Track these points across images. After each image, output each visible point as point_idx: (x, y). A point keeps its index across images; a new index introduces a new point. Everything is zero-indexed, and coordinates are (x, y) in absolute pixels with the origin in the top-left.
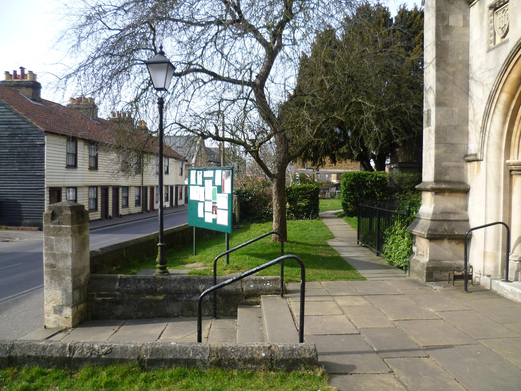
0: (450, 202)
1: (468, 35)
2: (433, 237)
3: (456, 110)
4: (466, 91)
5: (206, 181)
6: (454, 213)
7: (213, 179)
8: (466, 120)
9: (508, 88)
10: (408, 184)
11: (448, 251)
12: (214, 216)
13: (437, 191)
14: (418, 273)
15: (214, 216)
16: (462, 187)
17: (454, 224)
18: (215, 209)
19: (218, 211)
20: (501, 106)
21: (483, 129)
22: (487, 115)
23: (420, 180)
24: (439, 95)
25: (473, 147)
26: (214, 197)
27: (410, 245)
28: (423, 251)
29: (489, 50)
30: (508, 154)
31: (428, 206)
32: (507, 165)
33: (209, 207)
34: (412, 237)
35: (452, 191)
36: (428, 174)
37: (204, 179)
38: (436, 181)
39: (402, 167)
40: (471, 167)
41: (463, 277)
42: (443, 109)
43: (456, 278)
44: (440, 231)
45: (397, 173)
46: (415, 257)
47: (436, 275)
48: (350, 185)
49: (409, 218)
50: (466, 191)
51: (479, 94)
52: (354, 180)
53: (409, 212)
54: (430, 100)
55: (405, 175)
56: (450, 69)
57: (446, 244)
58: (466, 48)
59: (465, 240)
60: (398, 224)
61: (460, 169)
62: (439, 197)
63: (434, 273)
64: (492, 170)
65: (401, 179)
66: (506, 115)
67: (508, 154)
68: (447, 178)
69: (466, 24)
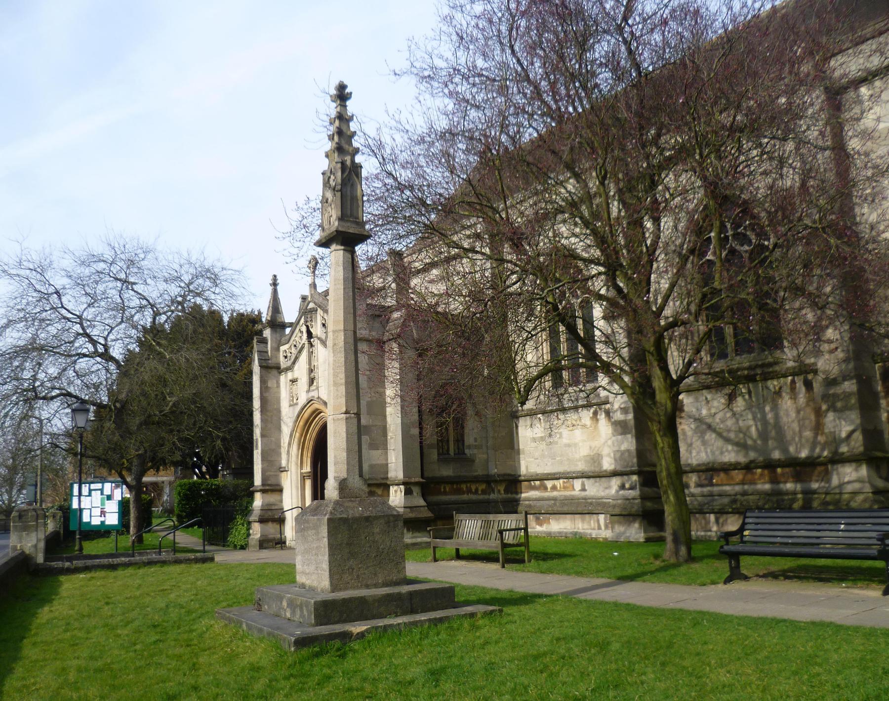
0: (272, 498)
1: (279, 393)
2: (262, 521)
3: (273, 439)
4: (279, 429)
5: (93, 492)
6: (274, 505)
7: (102, 490)
8: (279, 446)
9: (299, 430)
10: (243, 490)
11: (272, 529)
12: (103, 519)
13: (263, 491)
14: (254, 546)
15: (103, 519)
16: (278, 488)
17: (274, 512)
18: (103, 513)
19: (107, 515)
20: (296, 440)
21: (288, 452)
22: (289, 444)
23: (252, 484)
24: (263, 429)
25: (284, 463)
26: (103, 504)
27: (248, 529)
28: (257, 531)
29: (290, 406)
30: (301, 468)
31: (258, 501)
32: (301, 473)
33: (96, 512)
34: (249, 523)
35: (273, 491)
36: (258, 481)
37: (90, 491)
38: (263, 485)
39: (236, 473)
40: (283, 474)
41: (280, 543)
42: (265, 439)
43: (276, 544)
44: (266, 516)
45: (229, 478)
46: (251, 537)
47: (265, 545)
48: (185, 495)
49: (246, 511)
50: (281, 491)
51: (286, 430)
52: (190, 489)
53: (247, 507)
54: (257, 432)
55: (240, 481)
56: (268, 414)
57: (270, 524)
58: (278, 401)
59: (281, 521)
60: (239, 517)
61: (277, 477)
62: (265, 495)
63: (264, 544)
64: (294, 477)
65: (236, 486)
66: (299, 445)
67: (301, 468)
68: (269, 482)
69: (278, 386)
